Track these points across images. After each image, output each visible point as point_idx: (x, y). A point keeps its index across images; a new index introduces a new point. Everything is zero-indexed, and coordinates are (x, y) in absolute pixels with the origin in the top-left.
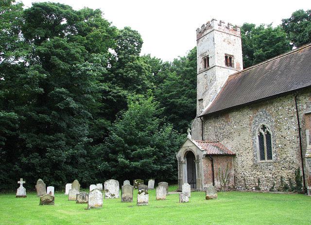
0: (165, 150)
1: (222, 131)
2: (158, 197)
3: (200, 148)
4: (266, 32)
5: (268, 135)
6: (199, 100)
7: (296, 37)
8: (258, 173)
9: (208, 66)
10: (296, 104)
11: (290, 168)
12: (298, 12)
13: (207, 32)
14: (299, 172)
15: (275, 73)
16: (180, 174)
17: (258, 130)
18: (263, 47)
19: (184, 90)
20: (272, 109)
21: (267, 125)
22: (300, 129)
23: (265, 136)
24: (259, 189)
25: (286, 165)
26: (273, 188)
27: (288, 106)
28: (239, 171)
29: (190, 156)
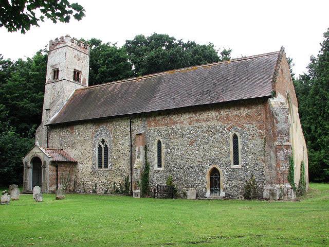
0: (6, 152)
2: (13, 198)
3: (47, 155)
4: (112, 50)
5: (106, 148)
6: (47, 110)
7: (136, 60)
8: (96, 179)
9: (57, 78)
10: (131, 125)
11: (121, 176)
12: (140, 36)
13: (60, 46)
14: (128, 179)
15: (117, 95)
16: (26, 177)
17: (98, 142)
18: (107, 64)
19: (27, 93)
20: (111, 126)
21: (105, 140)
22: (131, 145)
23: (103, 149)
24: (96, 192)
25: (119, 173)
26: (107, 191)
27: (124, 126)
28: (80, 176)
29: (37, 161)
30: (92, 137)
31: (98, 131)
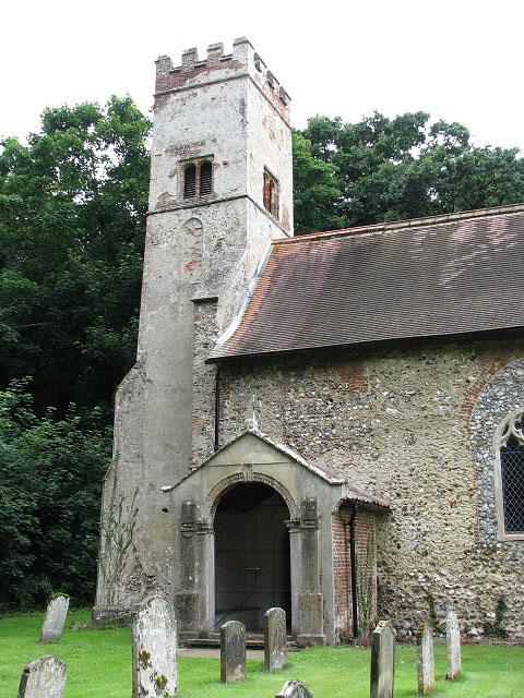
1: (323, 422)
8: (498, 577)
13: (213, 79)
24: (503, 634)
28: (405, 565)
30: (467, 407)
31: (500, 382)
